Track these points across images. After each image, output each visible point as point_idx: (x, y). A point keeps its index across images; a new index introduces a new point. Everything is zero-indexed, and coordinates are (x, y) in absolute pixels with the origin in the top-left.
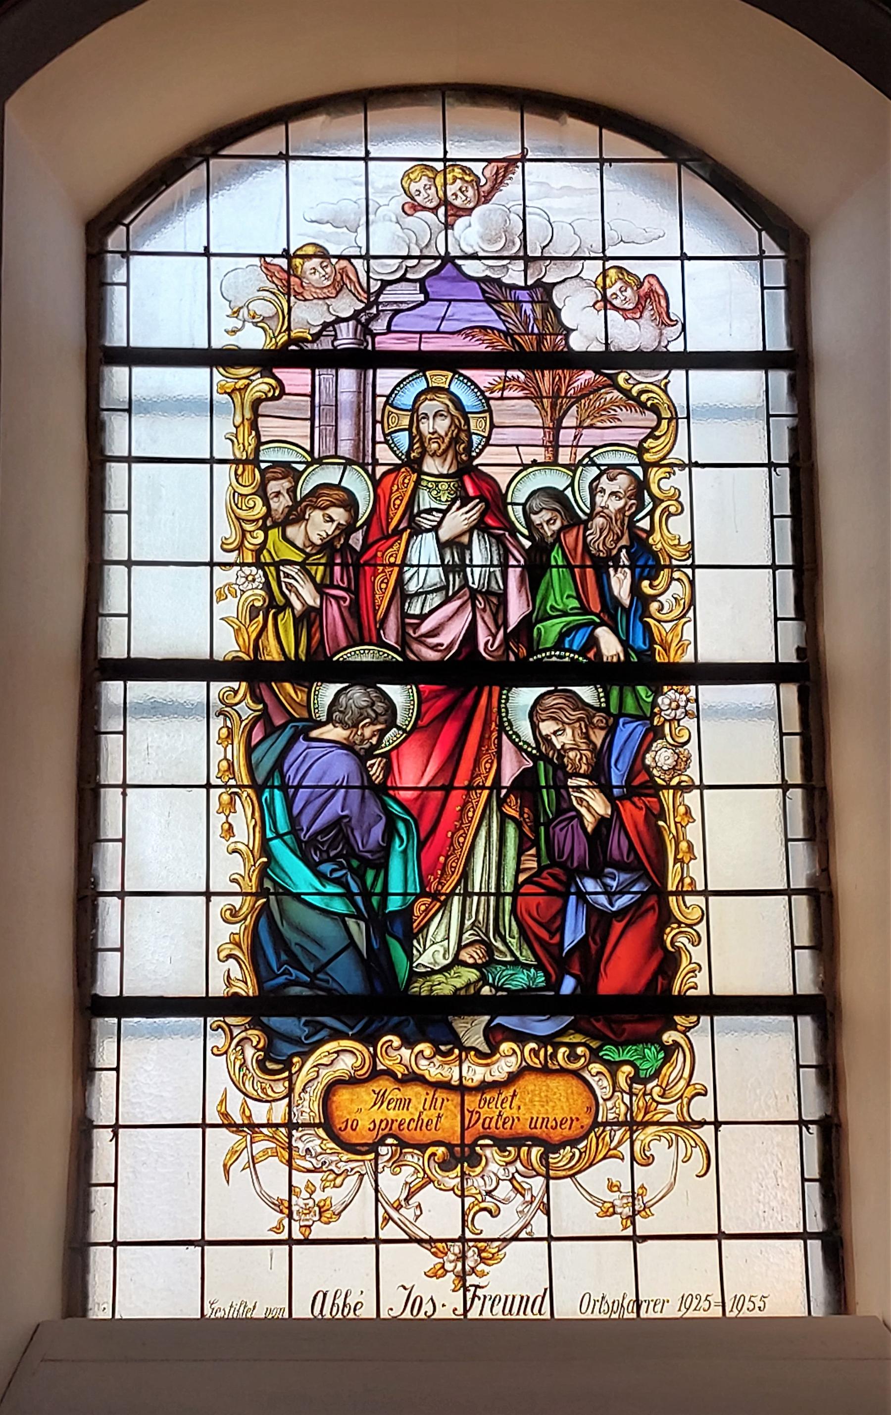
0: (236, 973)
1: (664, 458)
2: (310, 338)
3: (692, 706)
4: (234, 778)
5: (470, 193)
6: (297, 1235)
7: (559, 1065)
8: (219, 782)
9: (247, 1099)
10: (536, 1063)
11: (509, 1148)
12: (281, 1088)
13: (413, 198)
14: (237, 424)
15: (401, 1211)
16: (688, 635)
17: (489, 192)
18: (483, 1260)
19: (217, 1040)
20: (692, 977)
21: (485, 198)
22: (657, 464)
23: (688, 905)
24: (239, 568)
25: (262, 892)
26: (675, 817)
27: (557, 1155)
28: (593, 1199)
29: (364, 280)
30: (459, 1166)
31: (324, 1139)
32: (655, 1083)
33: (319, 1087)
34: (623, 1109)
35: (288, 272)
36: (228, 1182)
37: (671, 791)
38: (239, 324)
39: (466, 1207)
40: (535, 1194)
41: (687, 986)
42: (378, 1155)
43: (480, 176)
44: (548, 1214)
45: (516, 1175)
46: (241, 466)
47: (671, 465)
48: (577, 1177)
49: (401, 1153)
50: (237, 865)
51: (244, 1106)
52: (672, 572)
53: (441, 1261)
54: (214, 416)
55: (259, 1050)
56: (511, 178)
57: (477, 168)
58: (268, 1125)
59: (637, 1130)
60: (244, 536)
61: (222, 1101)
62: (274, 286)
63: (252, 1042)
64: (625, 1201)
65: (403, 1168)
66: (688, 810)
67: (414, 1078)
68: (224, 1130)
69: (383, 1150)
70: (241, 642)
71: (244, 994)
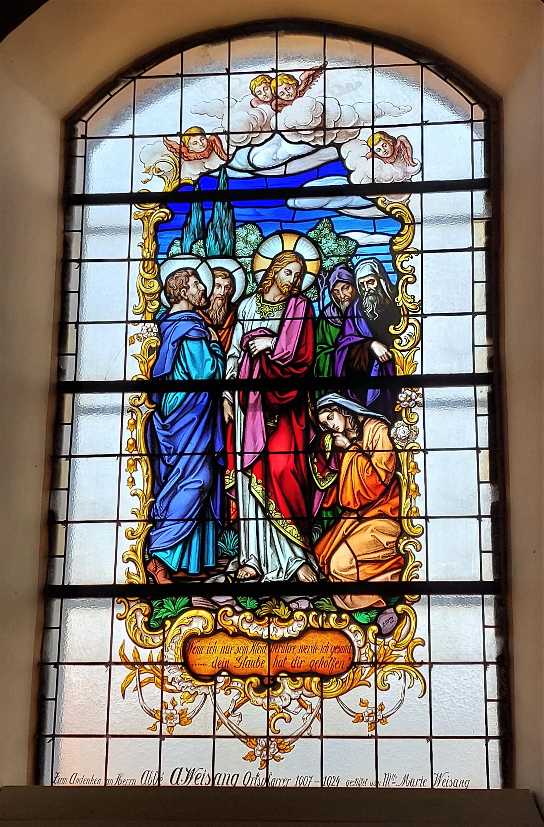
0: (133, 569)
1: (406, 248)
4: (137, 450)
5: (291, 91)
8: (127, 453)
9: (137, 647)
12: (158, 640)
13: (256, 96)
17: (303, 90)
21: (300, 94)
22: (402, 252)
26: (407, 470)
30: (267, 691)
34: (371, 654)
37: (406, 453)
39: (270, 716)
41: (411, 577)
42: (216, 682)
43: (299, 80)
45: (302, 696)
47: (410, 253)
48: (340, 697)
49: (231, 681)
51: (136, 652)
52: (408, 319)
57: (296, 75)
58: (150, 663)
60: (147, 304)
61: (122, 646)
62: (172, 154)
63: (142, 611)
64: (370, 712)
66: (416, 465)
67: (239, 634)
70: (143, 369)
71: (137, 583)
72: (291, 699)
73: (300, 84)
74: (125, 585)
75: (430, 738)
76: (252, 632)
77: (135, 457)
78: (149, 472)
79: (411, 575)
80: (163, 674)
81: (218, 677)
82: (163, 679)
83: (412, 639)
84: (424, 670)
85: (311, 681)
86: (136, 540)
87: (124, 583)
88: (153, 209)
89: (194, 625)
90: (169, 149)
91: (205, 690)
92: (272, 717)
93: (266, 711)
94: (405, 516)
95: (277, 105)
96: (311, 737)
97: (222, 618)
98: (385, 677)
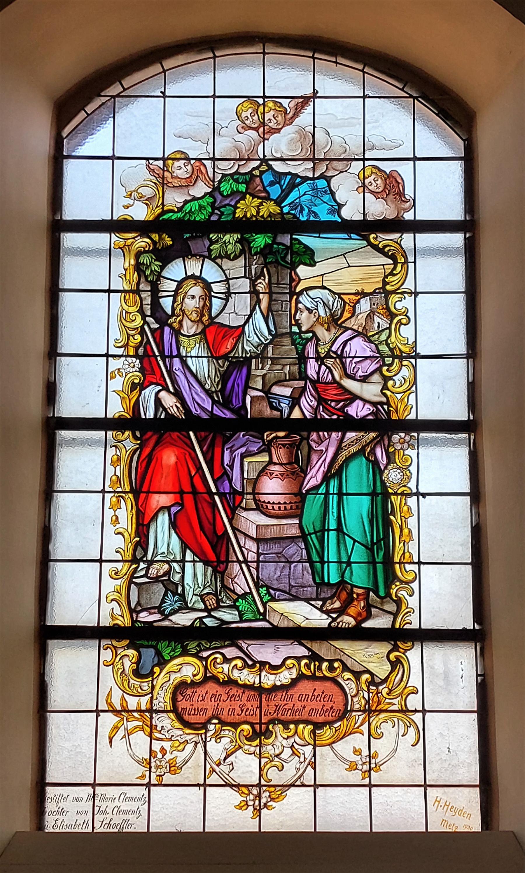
0: (117, 611)
1: (398, 289)
2: (176, 210)
5: (280, 118)
6: (154, 781)
8: (111, 490)
10: (308, 673)
12: (146, 687)
14: (126, 268)
18: (272, 799)
19: (107, 655)
22: (394, 292)
23: (407, 570)
24: (124, 358)
25: (135, 560)
28: (343, 760)
30: (259, 739)
31: (173, 720)
34: (363, 702)
35: (163, 170)
38: (131, 202)
44: (315, 769)
45: (295, 744)
46: (128, 294)
47: (402, 293)
55: (133, 663)
57: (285, 102)
60: (128, 339)
62: (155, 178)
65: (222, 739)
66: (409, 508)
68: (110, 714)
72: (284, 747)
73: (288, 112)
74: (109, 627)
75: (214, 96)
77: (119, 494)
78: (134, 511)
79: (404, 621)
80: (151, 722)
81: (209, 725)
82: (152, 727)
83: (405, 688)
84: (417, 718)
85: (304, 728)
86: (120, 580)
90: (151, 173)
92: (265, 767)
93: (258, 760)
94: (398, 561)
96: (303, 785)
97: (212, 666)
98: (379, 727)
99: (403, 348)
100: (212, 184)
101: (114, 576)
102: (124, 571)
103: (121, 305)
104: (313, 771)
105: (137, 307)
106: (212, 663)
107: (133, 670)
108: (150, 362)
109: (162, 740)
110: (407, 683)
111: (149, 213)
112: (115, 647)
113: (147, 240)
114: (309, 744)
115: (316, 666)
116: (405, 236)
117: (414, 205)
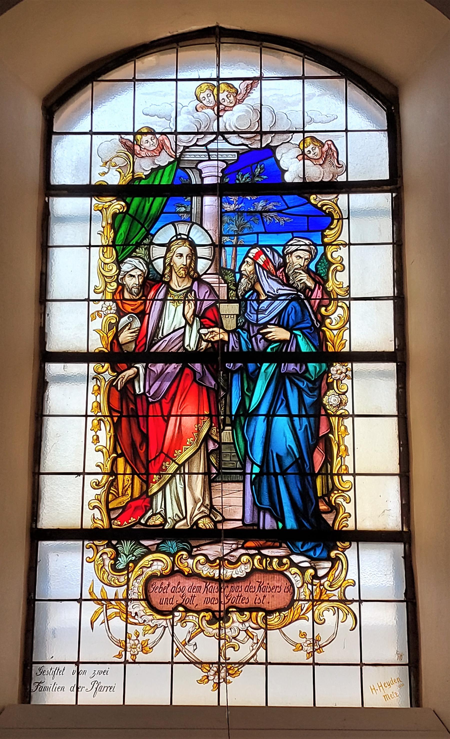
2: (144, 177)
3: (349, 373)
4: (101, 412)
5: (232, 98)
7: (273, 568)
8: (93, 414)
11: (245, 613)
15: (186, 647)
16: (346, 336)
19: (89, 553)
20: (345, 521)
21: (240, 101)
22: (330, 244)
26: (338, 432)
27: (272, 617)
29: (174, 147)
32: (326, 579)
33: (142, 579)
34: (308, 593)
36: (92, 629)
37: (337, 418)
38: (106, 170)
40: (259, 638)
44: (266, 649)
45: (249, 628)
46: (106, 248)
48: (282, 629)
50: (100, 458)
53: (206, 674)
54: (92, 222)
56: (254, 90)
57: (236, 84)
59: (316, 605)
60: (106, 286)
64: (308, 642)
66: (346, 428)
69: (176, 614)
70: (104, 343)
71: (102, 528)
72: (240, 630)
73: (239, 93)
74: (91, 530)
76: (205, 573)
79: (342, 524)
84: (354, 607)
87: (90, 528)
88: (110, 201)
89: (154, 568)
91: (164, 623)
93: (218, 641)
94: (336, 472)
95: (219, 111)
98: (321, 613)
99: (338, 291)
100: (174, 154)
101: (96, 487)
102: (104, 482)
103: (100, 258)
104: (265, 651)
105: (112, 259)
106: (179, 558)
107: (111, 564)
108: (333, 580)
109: (136, 624)
110: (345, 577)
111: (121, 178)
112: (96, 546)
113: (123, 203)
114: (262, 628)
115: (268, 562)
116: (341, 196)
117: (347, 170)
